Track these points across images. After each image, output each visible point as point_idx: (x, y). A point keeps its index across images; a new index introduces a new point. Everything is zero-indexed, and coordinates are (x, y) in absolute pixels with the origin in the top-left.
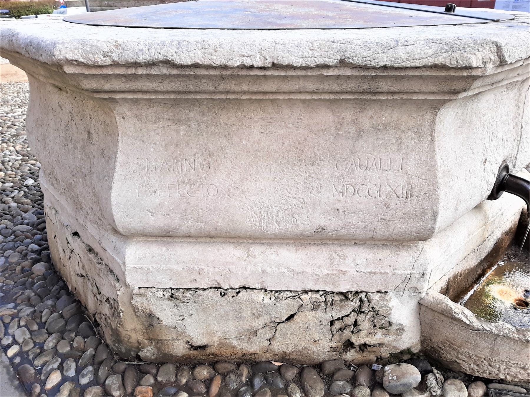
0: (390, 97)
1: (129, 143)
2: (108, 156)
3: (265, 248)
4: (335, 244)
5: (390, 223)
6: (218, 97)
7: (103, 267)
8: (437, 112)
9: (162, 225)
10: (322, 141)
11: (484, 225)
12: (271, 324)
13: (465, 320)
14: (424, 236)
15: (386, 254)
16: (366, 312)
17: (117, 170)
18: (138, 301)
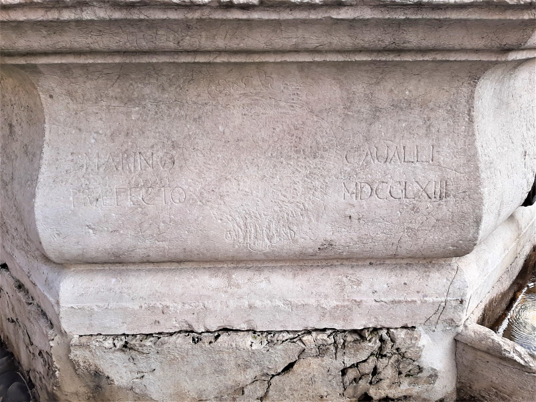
0: (420, 58)
1: (60, 132)
2: (32, 153)
3: (252, 273)
4: (345, 265)
5: (419, 234)
6: (183, 59)
7: (33, 309)
8: (476, 83)
9: (108, 246)
10: (327, 125)
11: (518, 238)
12: (263, 378)
13: (517, 358)
14: (462, 250)
15: (412, 276)
16: (388, 355)
17: (43, 170)
18: (78, 354)
